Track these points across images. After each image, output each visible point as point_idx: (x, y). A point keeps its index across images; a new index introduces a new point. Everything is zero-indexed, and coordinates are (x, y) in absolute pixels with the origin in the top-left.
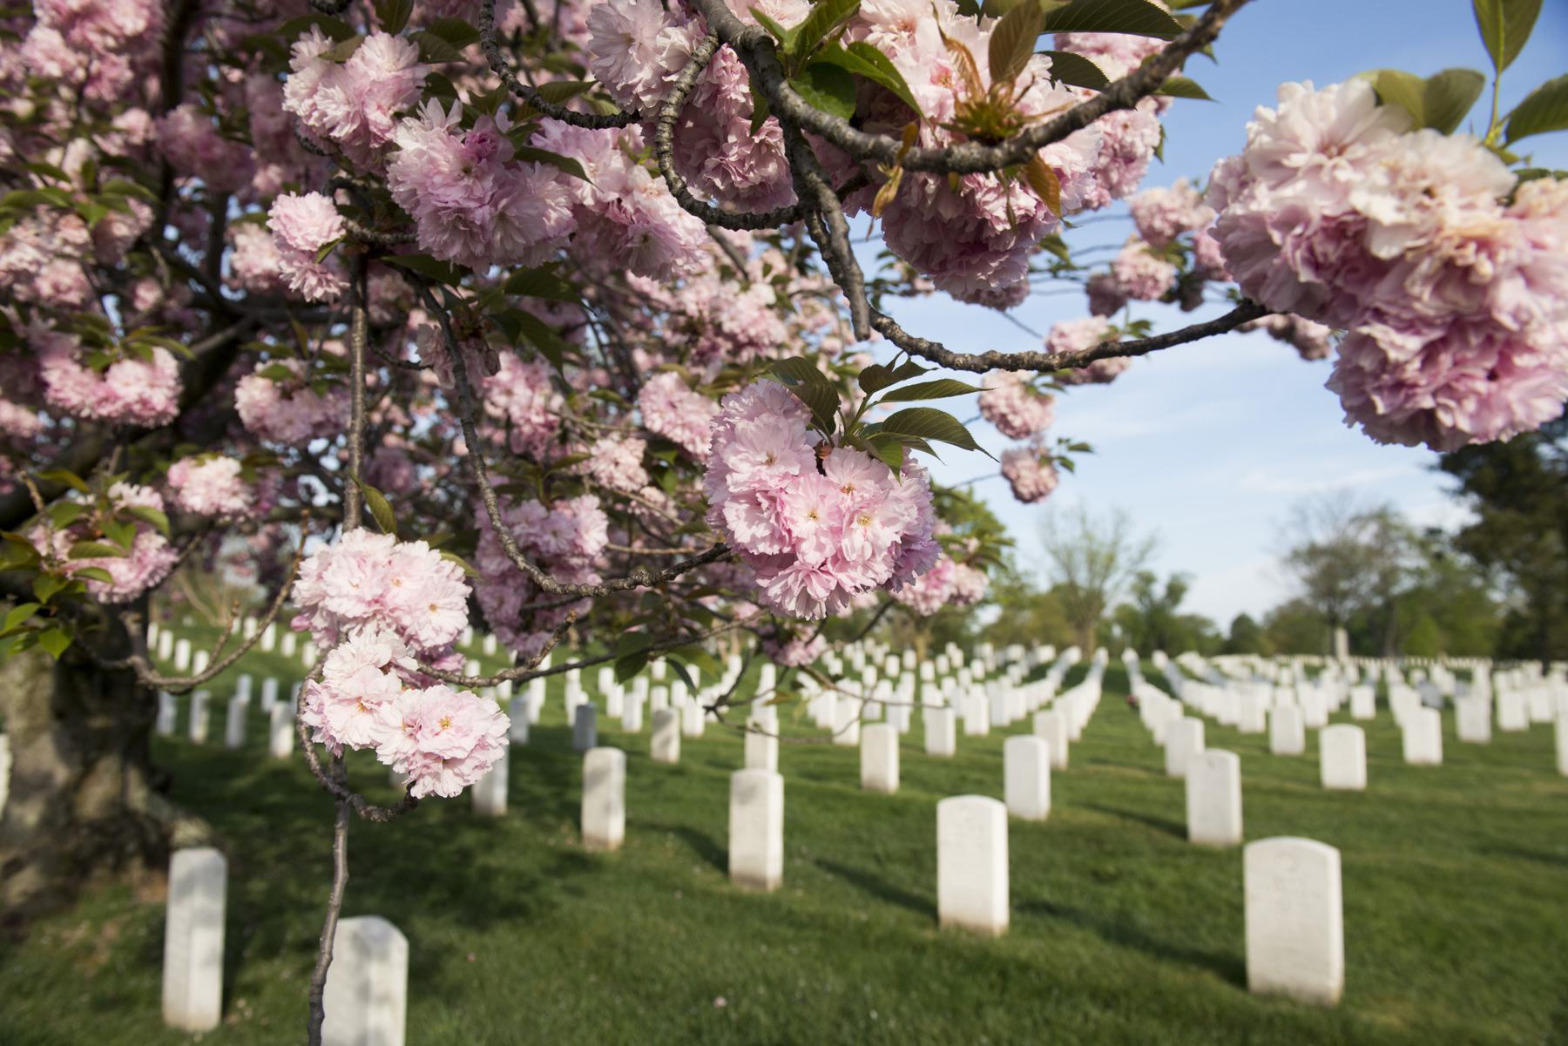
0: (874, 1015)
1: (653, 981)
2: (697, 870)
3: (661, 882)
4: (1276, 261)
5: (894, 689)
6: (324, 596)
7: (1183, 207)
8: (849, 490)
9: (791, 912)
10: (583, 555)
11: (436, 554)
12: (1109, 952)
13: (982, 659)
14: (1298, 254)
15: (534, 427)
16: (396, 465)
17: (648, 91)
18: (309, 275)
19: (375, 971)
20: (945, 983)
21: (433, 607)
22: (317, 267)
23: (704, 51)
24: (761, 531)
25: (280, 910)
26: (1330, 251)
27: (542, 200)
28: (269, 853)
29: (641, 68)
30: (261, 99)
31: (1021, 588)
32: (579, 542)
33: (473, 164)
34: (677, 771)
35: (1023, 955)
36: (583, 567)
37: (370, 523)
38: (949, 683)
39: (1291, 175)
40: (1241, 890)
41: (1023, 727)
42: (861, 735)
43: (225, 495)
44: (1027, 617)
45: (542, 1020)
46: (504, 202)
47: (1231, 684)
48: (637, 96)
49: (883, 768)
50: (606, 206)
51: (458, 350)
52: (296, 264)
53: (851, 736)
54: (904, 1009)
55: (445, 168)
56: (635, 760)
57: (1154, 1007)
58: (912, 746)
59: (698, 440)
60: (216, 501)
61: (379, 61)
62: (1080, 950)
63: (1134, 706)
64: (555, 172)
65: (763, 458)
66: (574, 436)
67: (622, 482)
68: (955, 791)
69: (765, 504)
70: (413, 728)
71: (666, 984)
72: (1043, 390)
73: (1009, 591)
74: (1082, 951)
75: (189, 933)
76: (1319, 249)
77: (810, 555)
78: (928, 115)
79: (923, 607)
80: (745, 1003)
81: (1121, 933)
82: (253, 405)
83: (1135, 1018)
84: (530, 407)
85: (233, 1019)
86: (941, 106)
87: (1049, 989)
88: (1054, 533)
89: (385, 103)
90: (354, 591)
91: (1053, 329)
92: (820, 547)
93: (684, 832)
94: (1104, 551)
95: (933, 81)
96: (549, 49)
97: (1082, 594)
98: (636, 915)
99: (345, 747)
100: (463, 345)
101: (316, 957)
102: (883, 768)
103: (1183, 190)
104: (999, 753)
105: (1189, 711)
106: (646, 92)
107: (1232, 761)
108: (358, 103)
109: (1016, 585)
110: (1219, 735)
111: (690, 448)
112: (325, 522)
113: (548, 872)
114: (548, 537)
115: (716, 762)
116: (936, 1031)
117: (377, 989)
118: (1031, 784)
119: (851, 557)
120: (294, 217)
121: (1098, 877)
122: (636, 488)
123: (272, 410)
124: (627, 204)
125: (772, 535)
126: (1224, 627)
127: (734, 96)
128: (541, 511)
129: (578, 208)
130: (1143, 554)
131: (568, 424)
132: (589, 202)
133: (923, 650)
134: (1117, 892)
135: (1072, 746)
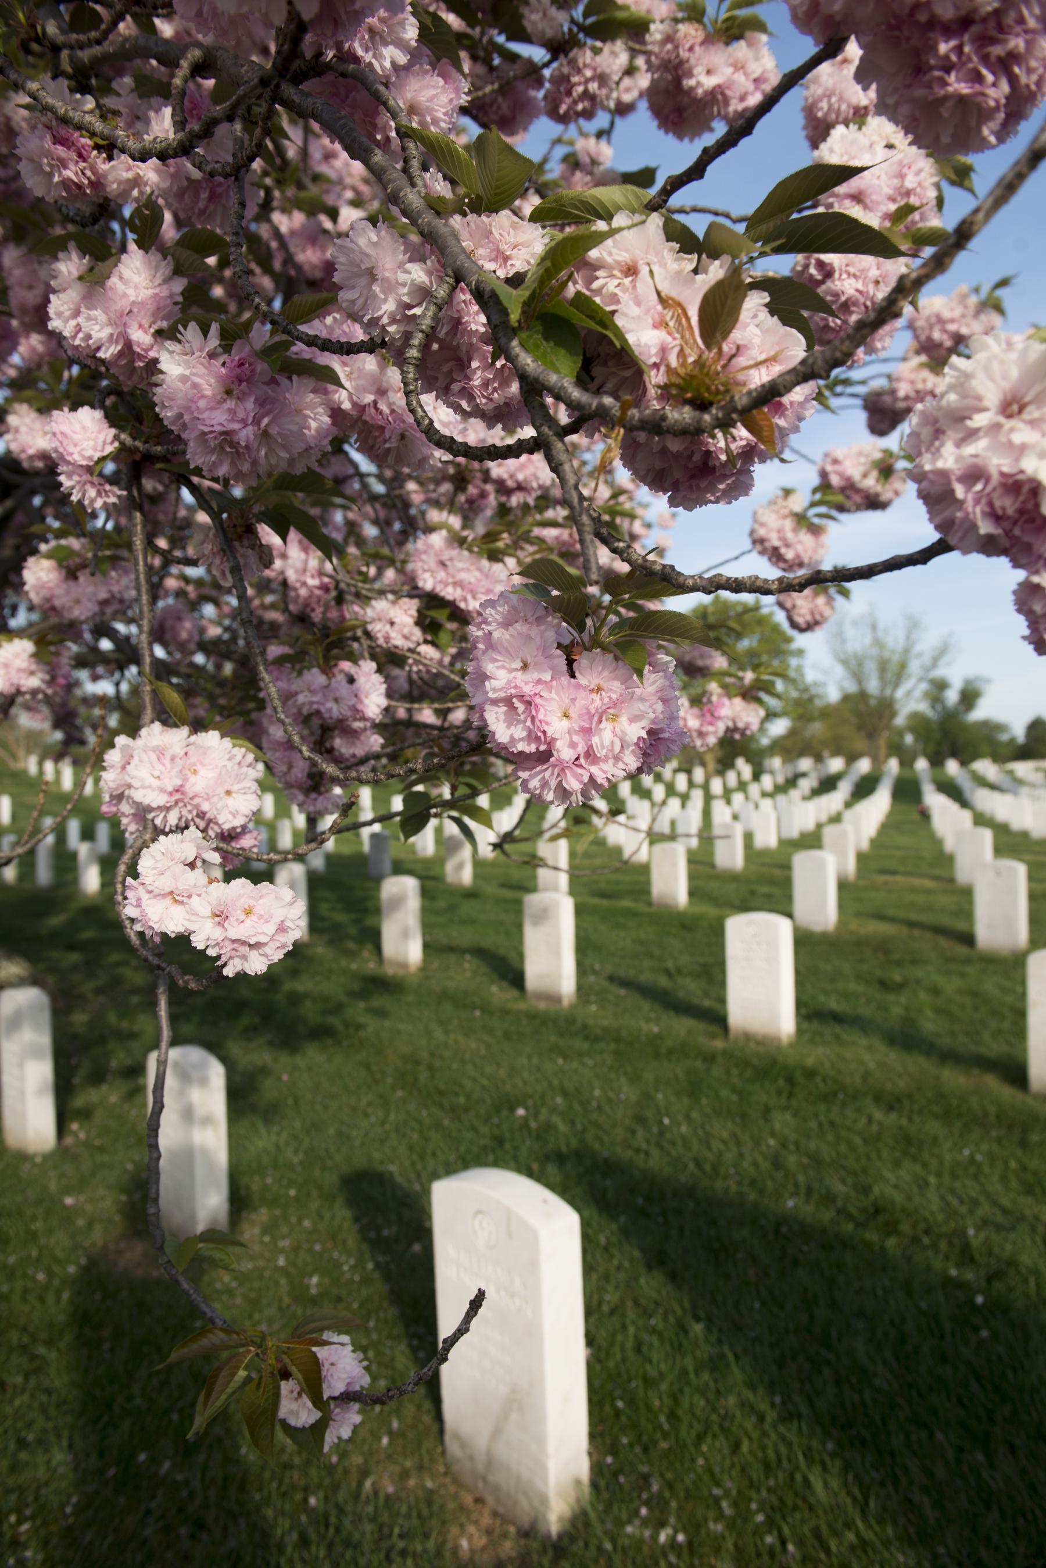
0: (666, 1121)
1: (457, 1094)
2: (494, 989)
3: (460, 1001)
4: (959, 514)
5: (683, 806)
6: (129, 786)
7: (963, 316)
8: (599, 689)
9: (585, 1027)
10: (364, 718)
11: (227, 742)
12: (894, 1057)
13: (772, 772)
14: (978, 509)
15: (310, 589)
16: (179, 619)
17: (393, 321)
18: (88, 487)
19: (196, 1095)
20: (734, 1090)
21: (228, 793)
22: (96, 480)
23: (442, 292)
24: (519, 732)
25: (103, 1040)
26: (1008, 505)
27: (298, 412)
28: (88, 987)
29: (385, 300)
30: (17, 272)
31: (811, 699)
32: (359, 707)
33: (234, 387)
34: (471, 894)
35: (810, 1062)
36: (365, 729)
37: (167, 719)
38: (738, 798)
39: (972, 434)
40: (1023, 996)
41: (811, 840)
42: (650, 853)
43: (23, 675)
44: (816, 729)
45: (354, 1133)
46: (265, 421)
47: (1024, 790)
48: (383, 327)
49: (672, 883)
50: (362, 409)
51: (232, 549)
52: (76, 478)
53: (643, 856)
54: (695, 1115)
55: (208, 392)
56: (430, 884)
57: (936, 1109)
58: (700, 863)
59: (469, 597)
60: (15, 681)
61: (136, 279)
62: (865, 1056)
63: (925, 815)
64: (310, 383)
65: (518, 664)
66: (349, 597)
67: (398, 641)
68: (745, 907)
69: (521, 707)
70: (220, 916)
71: (468, 1097)
72: (816, 521)
73: (798, 703)
74: (866, 1057)
75: (21, 1065)
76: (998, 504)
77: (564, 752)
80: (544, 1113)
81: (906, 1039)
82: (40, 587)
83: (917, 1119)
84: (305, 571)
85: (69, 1141)
86: (663, 350)
87: (835, 1094)
88: (843, 642)
89: (145, 323)
90: (156, 783)
91: (826, 455)
92: (573, 745)
93: (481, 953)
94: (896, 659)
96: (300, 186)
97: (873, 702)
98: (438, 1034)
99: (164, 935)
100: (237, 544)
101: (140, 1081)
102: (672, 883)
103: (963, 298)
104: (787, 867)
105: (981, 820)
106: (390, 324)
107: (1021, 870)
108: (121, 320)
109: (806, 696)
110: (1010, 842)
111: (462, 605)
112: (113, 666)
113: (353, 995)
114: (330, 704)
115: (512, 876)
116: (725, 1134)
117: (200, 1111)
118: (819, 893)
119: (601, 753)
120: (69, 433)
121: (884, 985)
122: (412, 646)
123: (59, 591)
124: (383, 407)
125: (529, 735)
126: (1018, 731)
127: (473, 327)
128: (322, 679)
129: (336, 413)
130: (935, 661)
131: (342, 585)
132: (346, 405)
133: (711, 765)
134: (903, 1000)
135: (861, 857)
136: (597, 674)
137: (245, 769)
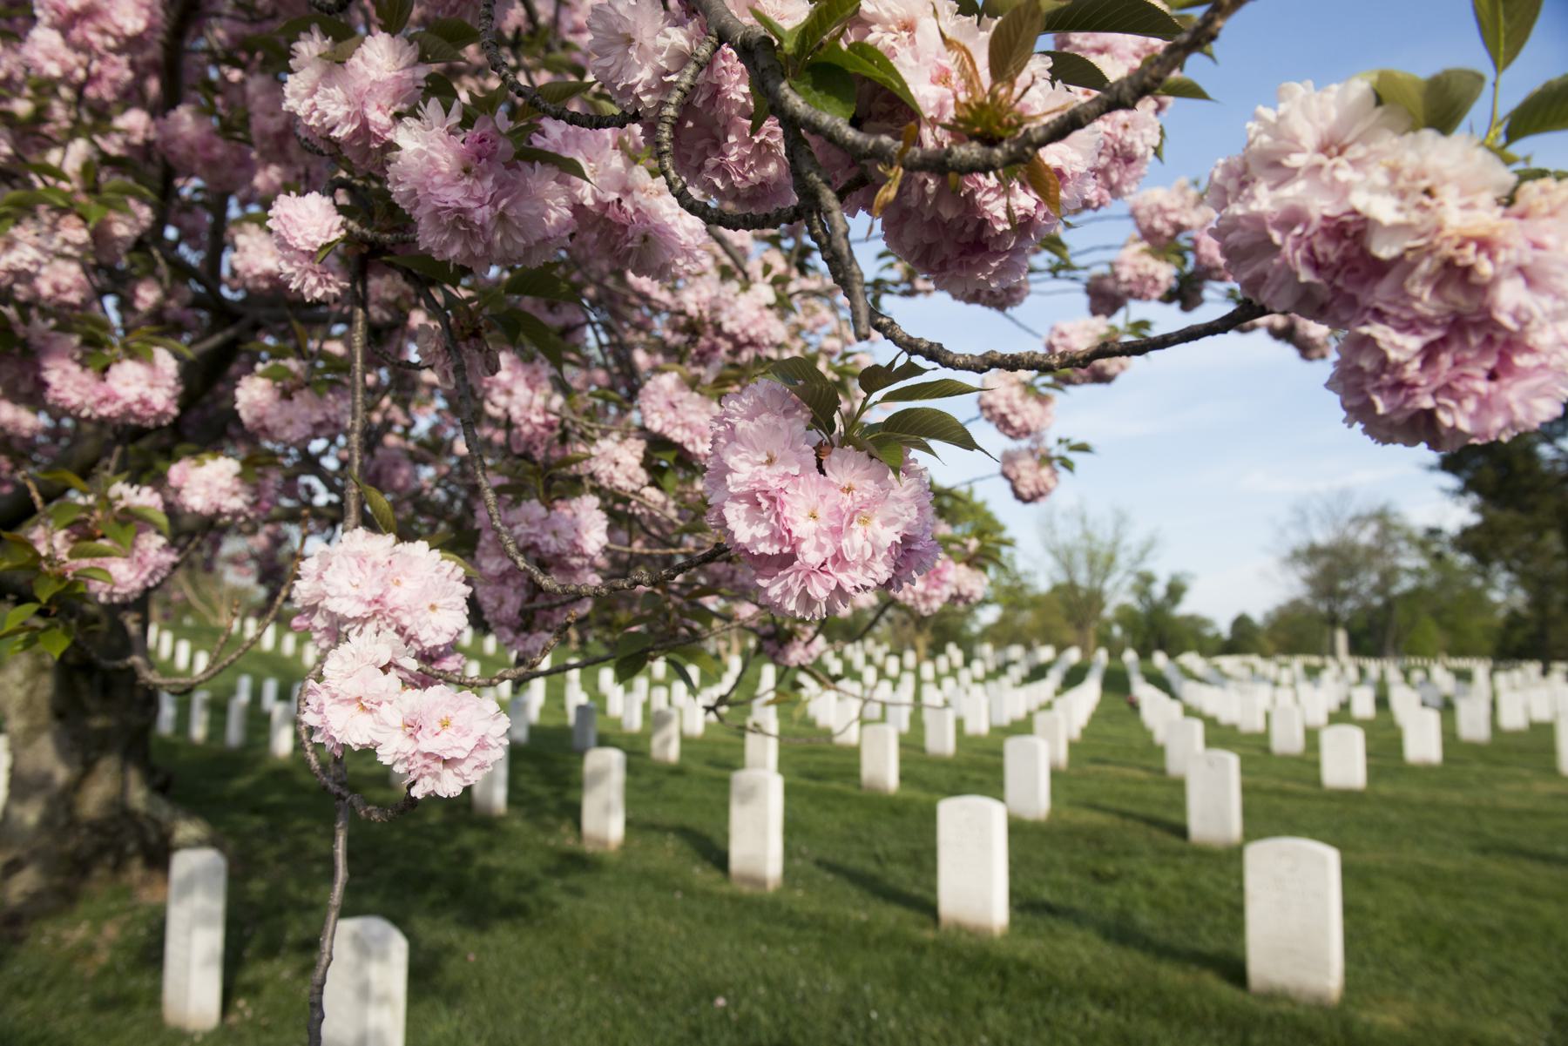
0: (874, 1015)
1: (653, 981)
2: (697, 870)
3: (661, 882)
4: (1276, 261)
5: (894, 689)
6: (324, 596)
7: (1183, 207)
8: (849, 490)
9: (791, 912)
10: (583, 555)
11: (436, 554)
12: (1109, 952)
13: (982, 659)
14: (1298, 254)
15: (534, 427)
16: (396, 465)
17: (648, 91)
18: (309, 275)
19: (375, 971)
20: (945, 983)
21: (433, 607)
22: (317, 267)
23: (704, 51)
24: (761, 531)
25: (280, 910)
26: (1330, 251)
27: (542, 200)
28: (269, 853)
29: (641, 68)
30: (261, 99)
31: (1021, 588)
32: (579, 542)
33: (473, 164)
34: (677, 771)
35: (1023, 955)
36: (583, 567)
37: (370, 523)
38: (949, 683)
39: (1291, 175)
40: (1241, 890)
41: (1023, 727)
42: (861, 735)
43: (225, 495)
44: (1027, 617)
45: (542, 1020)
46: (504, 202)
47: (1231, 684)
48: (637, 96)
49: (883, 768)
50: (606, 206)
51: (458, 350)
52: (296, 264)
53: (851, 736)
54: (904, 1009)
55: (445, 168)
56: (635, 760)
57: (1154, 1007)
58: (912, 746)
59: (698, 440)
60: (216, 501)
61: (379, 61)
62: (1080, 950)
63: (1134, 706)
64: (555, 172)
65: (763, 458)
66: (574, 436)
67: (622, 482)
68: (955, 791)
69: (765, 504)
70: (413, 728)
71: (666, 984)
72: (1043, 390)
73: (1009, 591)
74: (1082, 951)
75: (189, 933)
76: (1319, 249)
77: (810, 555)
80: (745, 1003)
81: (1121, 933)
82: (253, 405)
83: (1135, 1018)
84: (530, 407)
85: (233, 1019)
86: (941, 106)
87: (1049, 989)
88: (1054, 533)
89: (385, 103)
90: (354, 591)
91: (1053, 329)
92: (820, 547)
93: (684, 832)
94: (1104, 551)
95: (933, 81)
96: (549, 49)
97: (1082, 594)
98: (636, 915)
99: (345, 747)
100: (463, 345)
101: (316, 957)
102: (883, 768)
103: (1183, 190)
104: (999, 753)
105: (1189, 711)
106: (646, 92)
107: (1232, 761)
108: (358, 103)
109: (1016, 585)
110: (1219, 735)
111: (690, 448)
112: (325, 522)
113: (548, 872)
114: (548, 537)
115: (716, 762)
116: (936, 1031)
117: (377, 989)
118: (1031, 784)
119: (851, 557)
120: (294, 217)
121: (1098, 877)
122: (636, 488)
123: (272, 410)
124: (627, 204)
125: (772, 535)
126: (1224, 627)
127: (734, 96)
128: (541, 511)
129: (578, 208)
130: (1143, 554)
131: (568, 424)
132: (589, 202)
133: (923, 650)
134: (1117, 892)
135: (1072, 746)
136: (848, 471)
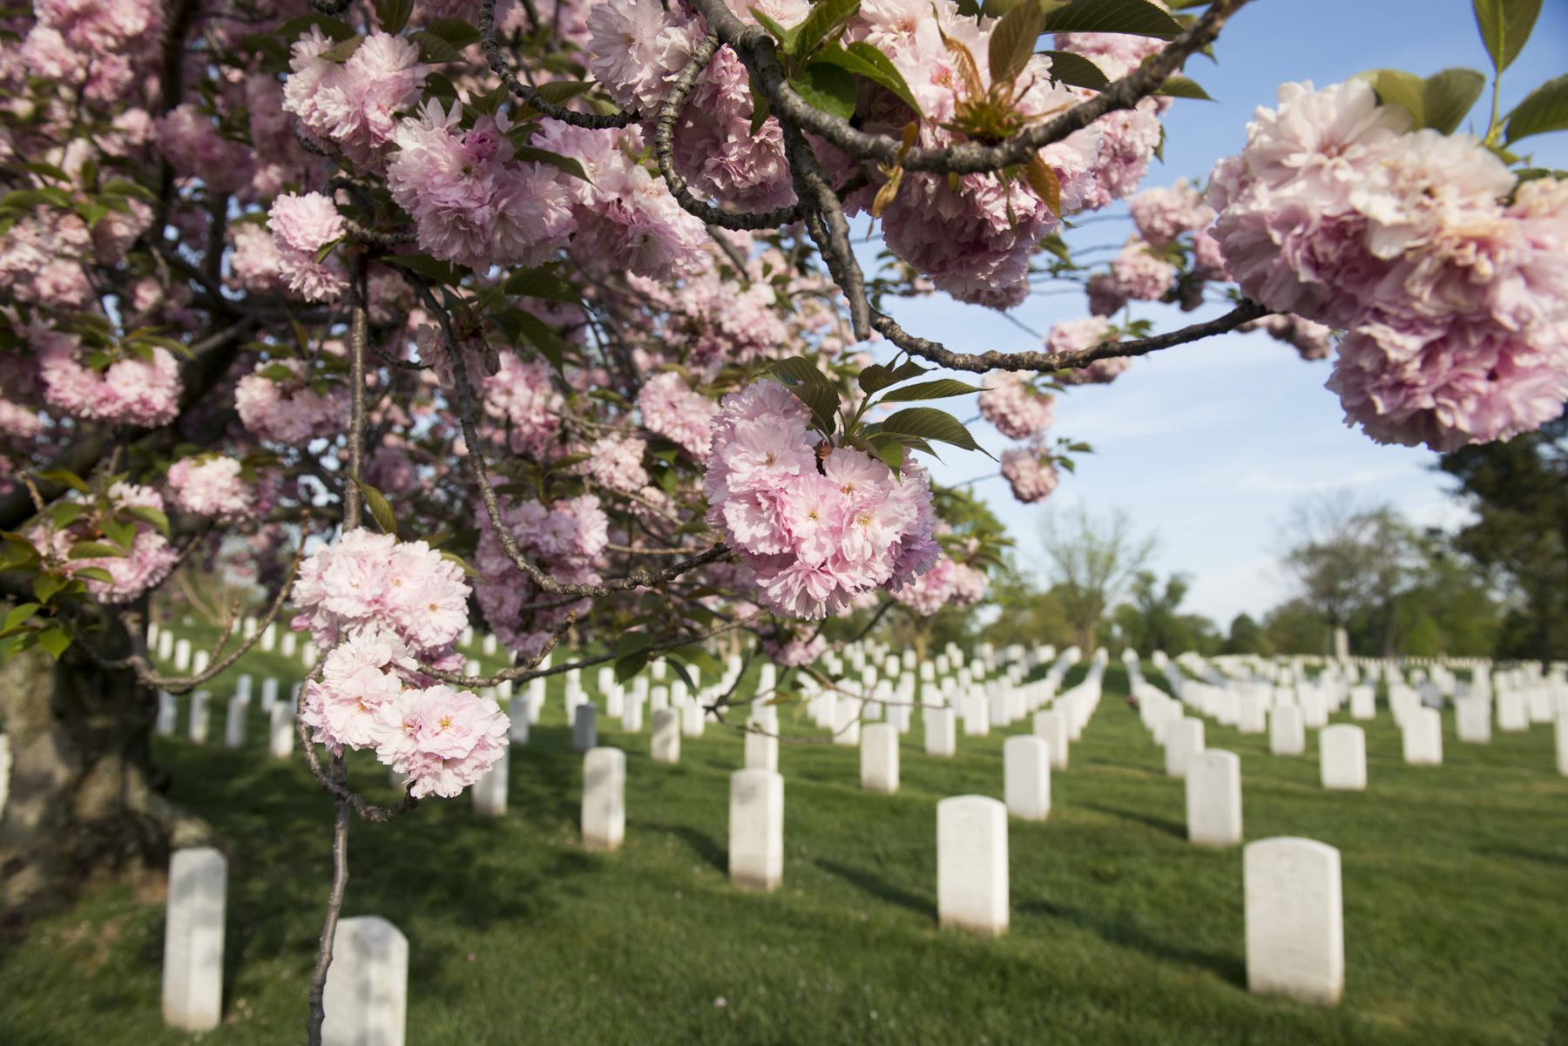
0: (874, 1015)
1: (653, 981)
2: (697, 870)
3: (661, 882)
4: (1276, 261)
5: (894, 689)
6: (324, 596)
7: (1183, 207)
8: (849, 490)
9: (791, 912)
10: (583, 555)
11: (436, 554)
12: (1109, 952)
13: (982, 659)
14: (1298, 254)
15: (534, 427)
16: (396, 465)
17: (648, 91)
18: (309, 275)
19: (375, 971)
20: (945, 983)
21: (433, 607)
23: (704, 51)
24: (761, 531)
25: (280, 910)
26: (1330, 251)
27: (542, 200)
28: (269, 853)
29: (641, 68)
30: (261, 99)
31: (1021, 588)
32: (579, 542)
33: (473, 164)
34: (677, 771)
35: (1023, 955)
36: (583, 567)
37: (370, 523)
38: (949, 683)
39: (1291, 175)
40: (1241, 890)
41: (1023, 727)
42: (861, 735)
43: (225, 495)
44: (1027, 617)
45: (542, 1020)
46: (504, 202)
47: (1231, 684)
48: (637, 96)
49: (883, 768)
50: (606, 206)
51: (458, 350)
52: (296, 264)
53: (851, 736)
54: (904, 1009)
55: (445, 168)
56: (635, 760)
57: (1154, 1007)
58: (912, 746)
59: (698, 440)
60: (216, 501)
61: (379, 61)
62: (1080, 950)
63: (1134, 706)
64: (555, 172)
65: (763, 458)
66: (574, 436)
67: (622, 482)
68: (955, 791)
69: (765, 504)
70: (413, 728)
71: (666, 984)
72: (1043, 390)
73: (1009, 591)
74: (1082, 951)
75: (189, 933)
76: (1319, 249)
77: (810, 555)
78: (928, 115)
79: (923, 607)
80: (745, 1003)
81: (1121, 933)
82: (253, 405)
83: (1135, 1018)
84: (530, 407)
85: (233, 1019)
86: (941, 106)
87: (1049, 989)
88: (1054, 533)
89: (385, 103)
90: (354, 591)
91: (1053, 329)
92: (820, 547)
93: (684, 832)
94: (1104, 551)
96: (549, 49)
97: (1082, 594)
98: (636, 915)
99: (345, 747)
100: (463, 345)
101: (316, 957)
102: (883, 768)
103: (1183, 190)
104: (999, 753)
105: (1189, 711)
106: (646, 92)
107: (1232, 761)
108: (358, 103)
109: (1016, 585)
110: (1219, 735)
111: (690, 448)
112: (325, 522)
113: (548, 872)
114: (548, 537)
115: (716, 762)
116: (936, 1031)
117: (377, 989)
118: (1031, 784)
119: (851, 557)
120: (294, 217)
121: (1098, 877)
122: (636, 488)
123: (272, 410)
124: (627, 204)
125: (772, 535)
126: (1224, 627)
127: (734, 96)
128: (541, 511)
129: (578, 208)
130: (1143, 554)
131: (568, 424)
132: (589, 202)
133: (923, 650)
134: (1117, 892)
135: (1072, 746)
136: (848, 471)
137: (452, 583)
